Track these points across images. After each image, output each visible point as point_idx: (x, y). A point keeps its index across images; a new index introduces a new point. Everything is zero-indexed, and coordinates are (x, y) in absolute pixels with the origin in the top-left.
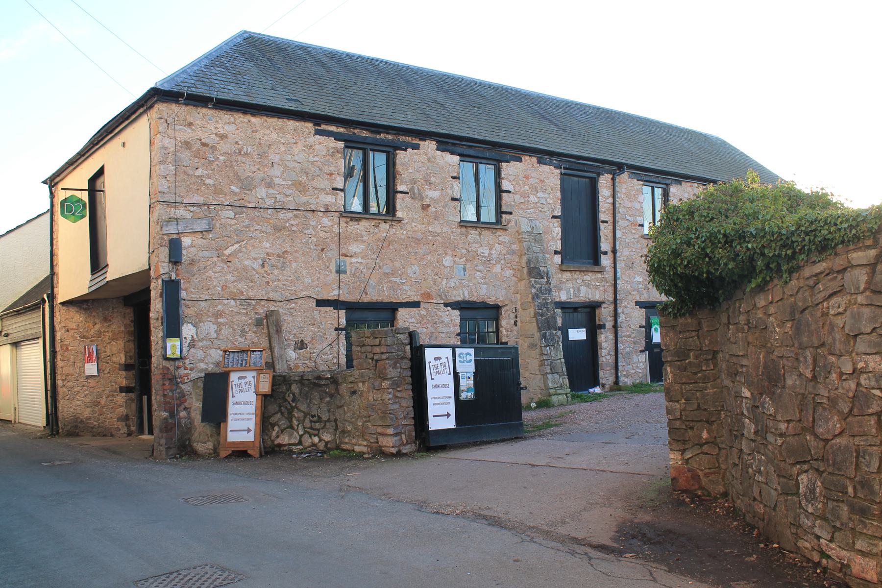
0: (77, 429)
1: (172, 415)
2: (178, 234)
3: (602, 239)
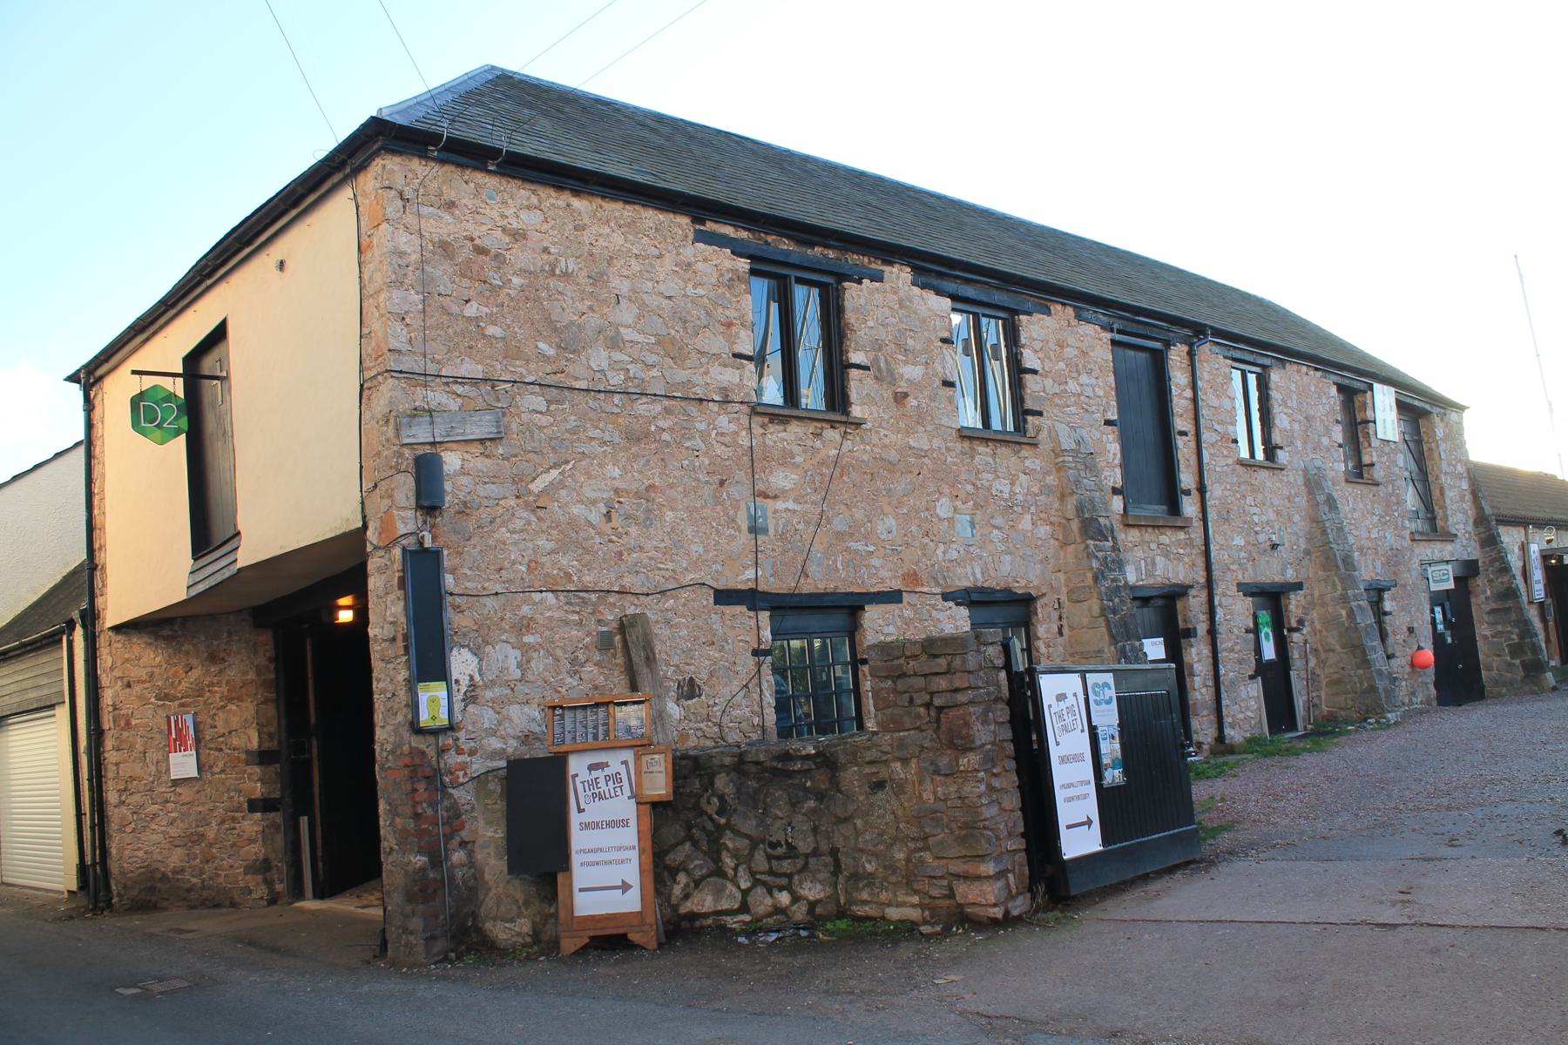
0: (154, 894)
1: (436, 860)
2: (433, 444)
3: (1182, 467)
